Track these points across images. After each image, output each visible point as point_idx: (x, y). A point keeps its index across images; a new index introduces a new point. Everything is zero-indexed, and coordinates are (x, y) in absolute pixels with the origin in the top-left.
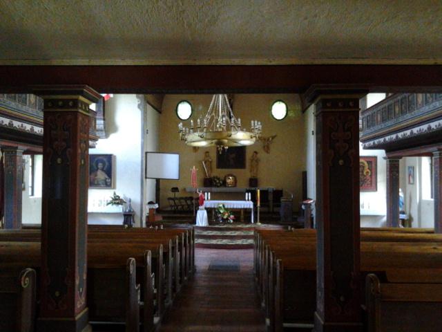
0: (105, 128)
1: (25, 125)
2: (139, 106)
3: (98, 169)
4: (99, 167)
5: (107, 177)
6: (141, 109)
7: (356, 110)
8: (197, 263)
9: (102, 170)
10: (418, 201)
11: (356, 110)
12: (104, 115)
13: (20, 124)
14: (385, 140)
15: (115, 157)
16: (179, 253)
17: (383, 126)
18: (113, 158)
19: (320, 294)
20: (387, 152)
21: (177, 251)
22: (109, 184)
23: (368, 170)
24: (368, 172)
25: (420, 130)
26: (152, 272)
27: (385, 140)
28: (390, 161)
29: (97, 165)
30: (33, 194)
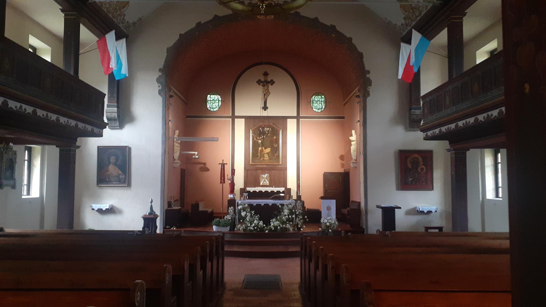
0: (118, 116)
1: (50, 114)
2: (160, 93)
3: (110, 163)
4: (111, 161)
5: (120, 172)
6: (162, 96)
7: (462, 21)
8: (227, 278)
9: (115, 164)
10: (481, 199)
11: (462, 21)
12: (118, 103)
13: (45, 113)
14: (457, 126)
15: (130, 149)
16: (201, 273)
17: (454, 109)
18: (32, 148)
19: (335, 3)
20: (450, 143)
21: (208, 260)
22: (122, 181)
23: (423, 167)
24: (422, 169)
25: (448, 128)
26: (201, 269)
27: (457, 126)
28: (456, 154)
29: (109, 159)
30: (28, 193)
